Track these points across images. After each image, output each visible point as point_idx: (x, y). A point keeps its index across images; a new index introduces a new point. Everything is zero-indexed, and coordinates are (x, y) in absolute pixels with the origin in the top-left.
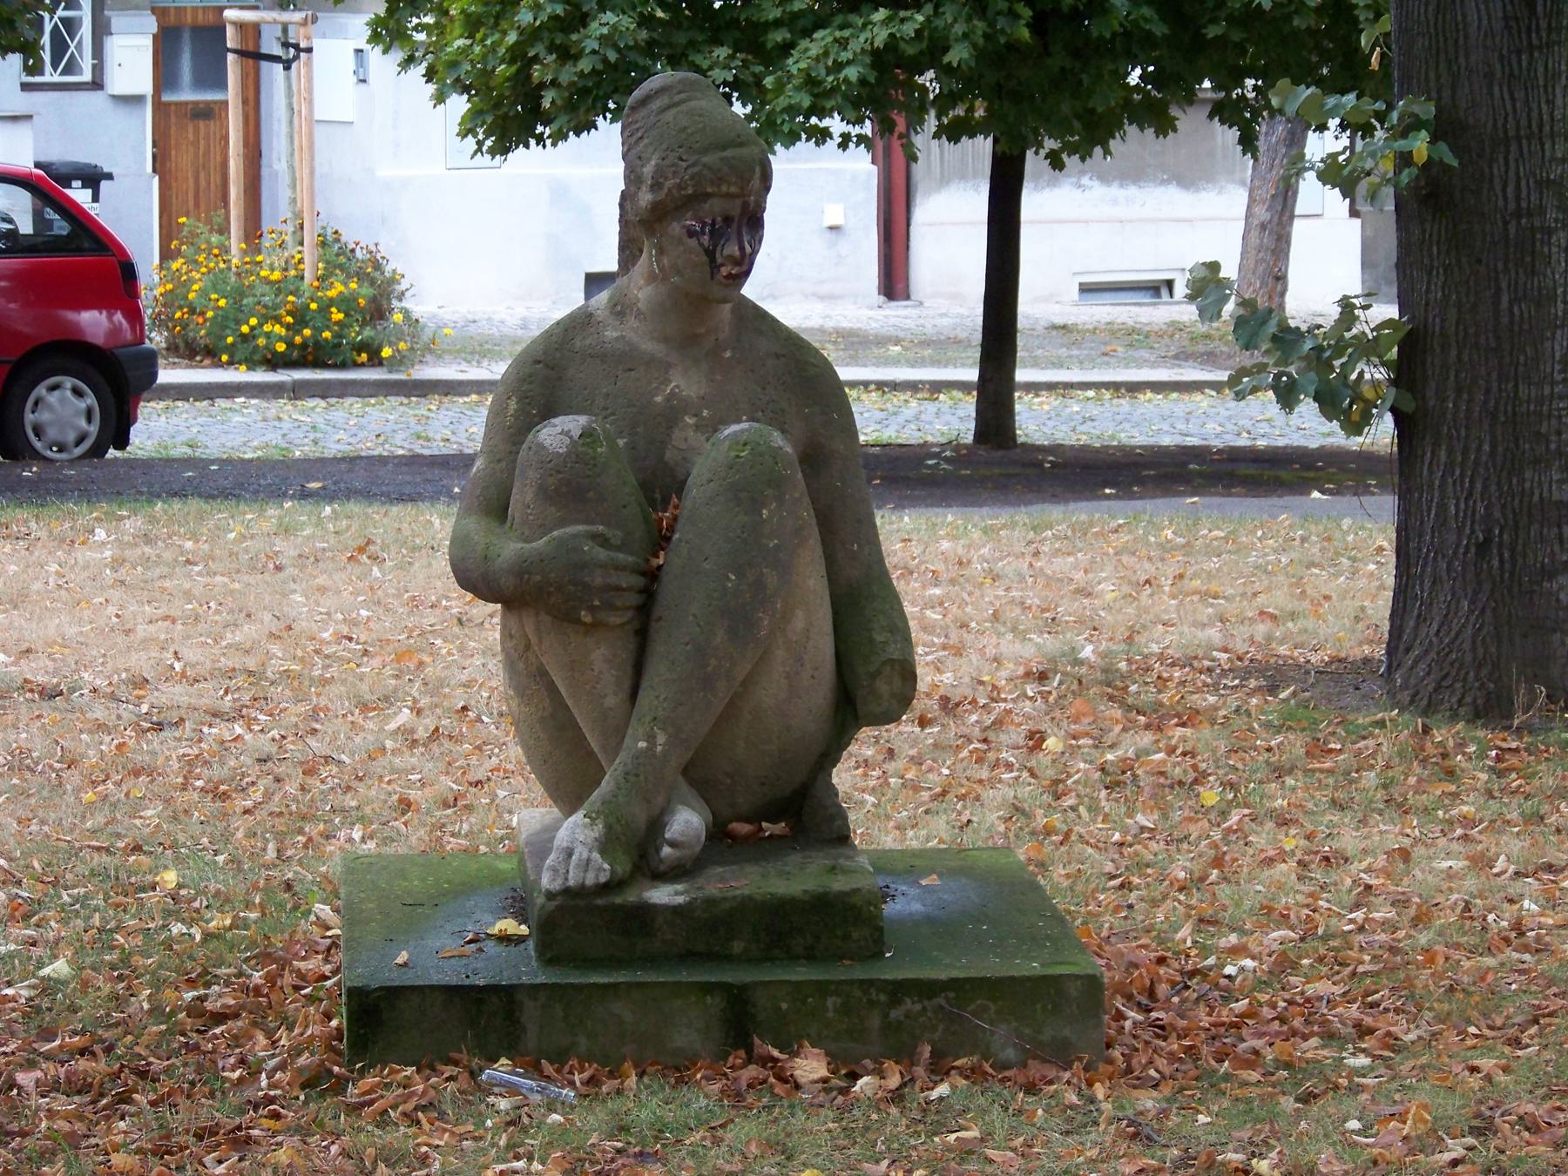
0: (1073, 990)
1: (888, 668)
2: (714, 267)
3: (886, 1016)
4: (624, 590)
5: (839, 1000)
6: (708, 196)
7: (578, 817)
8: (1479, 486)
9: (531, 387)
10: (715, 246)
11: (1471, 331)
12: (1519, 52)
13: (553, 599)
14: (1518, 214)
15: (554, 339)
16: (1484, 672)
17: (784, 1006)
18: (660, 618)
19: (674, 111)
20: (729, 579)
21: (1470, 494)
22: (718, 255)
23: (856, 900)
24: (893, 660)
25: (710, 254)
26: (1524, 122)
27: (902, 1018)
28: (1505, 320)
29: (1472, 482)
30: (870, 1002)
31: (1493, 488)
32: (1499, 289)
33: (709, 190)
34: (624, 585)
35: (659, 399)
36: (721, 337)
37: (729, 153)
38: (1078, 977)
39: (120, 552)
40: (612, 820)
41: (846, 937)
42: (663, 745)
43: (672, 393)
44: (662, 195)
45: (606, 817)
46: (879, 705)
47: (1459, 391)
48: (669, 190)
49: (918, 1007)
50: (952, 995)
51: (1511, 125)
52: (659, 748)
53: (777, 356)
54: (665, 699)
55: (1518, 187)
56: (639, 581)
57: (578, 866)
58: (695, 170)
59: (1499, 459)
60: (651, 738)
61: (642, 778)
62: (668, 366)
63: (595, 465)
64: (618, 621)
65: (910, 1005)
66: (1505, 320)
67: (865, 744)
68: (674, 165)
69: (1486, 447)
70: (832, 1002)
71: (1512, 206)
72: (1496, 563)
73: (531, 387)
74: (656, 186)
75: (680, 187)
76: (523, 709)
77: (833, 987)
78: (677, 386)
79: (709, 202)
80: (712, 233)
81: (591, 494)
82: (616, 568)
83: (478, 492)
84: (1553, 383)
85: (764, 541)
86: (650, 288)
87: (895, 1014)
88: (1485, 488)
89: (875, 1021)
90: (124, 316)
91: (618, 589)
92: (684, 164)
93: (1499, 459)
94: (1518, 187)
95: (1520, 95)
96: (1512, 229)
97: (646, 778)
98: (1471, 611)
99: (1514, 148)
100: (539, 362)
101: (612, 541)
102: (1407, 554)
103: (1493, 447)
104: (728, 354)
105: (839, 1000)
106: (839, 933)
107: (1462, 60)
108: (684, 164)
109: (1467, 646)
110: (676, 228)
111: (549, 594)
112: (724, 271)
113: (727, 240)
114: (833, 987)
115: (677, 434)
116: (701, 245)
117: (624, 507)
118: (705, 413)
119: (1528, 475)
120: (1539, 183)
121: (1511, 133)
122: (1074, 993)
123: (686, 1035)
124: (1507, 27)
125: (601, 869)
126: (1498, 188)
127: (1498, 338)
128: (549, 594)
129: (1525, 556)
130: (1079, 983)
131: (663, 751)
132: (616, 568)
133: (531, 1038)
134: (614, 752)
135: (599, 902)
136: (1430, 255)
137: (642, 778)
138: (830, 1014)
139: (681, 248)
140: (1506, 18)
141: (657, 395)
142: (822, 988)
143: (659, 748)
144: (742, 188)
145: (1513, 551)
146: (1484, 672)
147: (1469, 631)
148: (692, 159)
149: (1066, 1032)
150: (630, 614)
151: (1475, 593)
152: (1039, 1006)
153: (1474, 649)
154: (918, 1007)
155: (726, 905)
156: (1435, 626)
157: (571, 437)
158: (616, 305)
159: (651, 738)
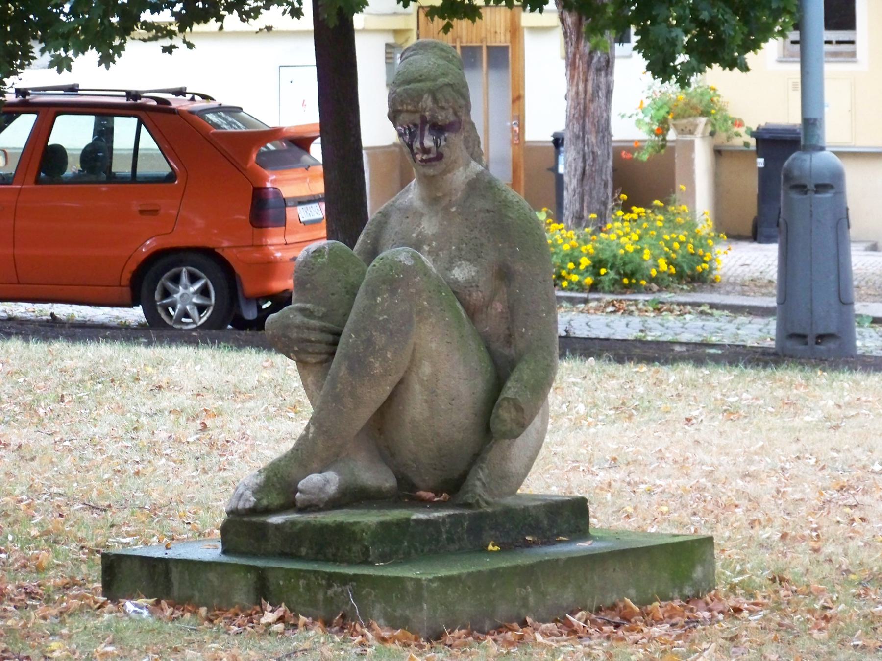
0: (410, 586)
1: (506, 403)
3: (326, 593)
4: (312, 342)
5: (305, 582)
10: (412, 142)
17: (281, 583)
20: (351, 337)
23: (357, 529)
24: (508, 398)
27: (333, 595)
30: (319, 584)
34: (313, 339)
35: (414, 235)
36: (454, 199)
37: (412, 86)
38: (411, 579)
40: (272, 474)
41: (350, 551)
42: (313, 433)
43: (421, 232)
45: (268, 472)
46: (504, 425)
49: (340, 590)
50: (355, 584)
52: (310, 435)
53: (488, 211)
56: (330, 338)
61: (300, 452)
62: (422, 215)
63: (313, 269)
64: (314, 361)
65: (336, 588)
70: (302, 582)
77: (302, 574)
78: (424, 228)
79: (402, 115)
80: (410, 133)
81: (308, 286)
82: (308, 329)
85: (377, 316)
87: (330, 593)
89: (321, 597)
90: (638, 206)
91: (310, 341)
97: (302, 452)
101: (316, 314)
104: (454, 209)
105: (305, 582)
106: (347, 547)
114: (302, 574)
117: (333, 294)
118: (434, 244)
122: (410, 589)
123: (241, 596)
125: (248, 500)
130: (412, 583)
131: (313, 436)
132: (308, 329)
133: (176, 591)
135: (245, 519)
137: (300, 452)
138: (301, 590)
141: (413, 233)
142: (298, 574)
143: (310, 435)
149: (407, 612)
152: (394, 595)
154: (340, 590)
155: (299, 526)
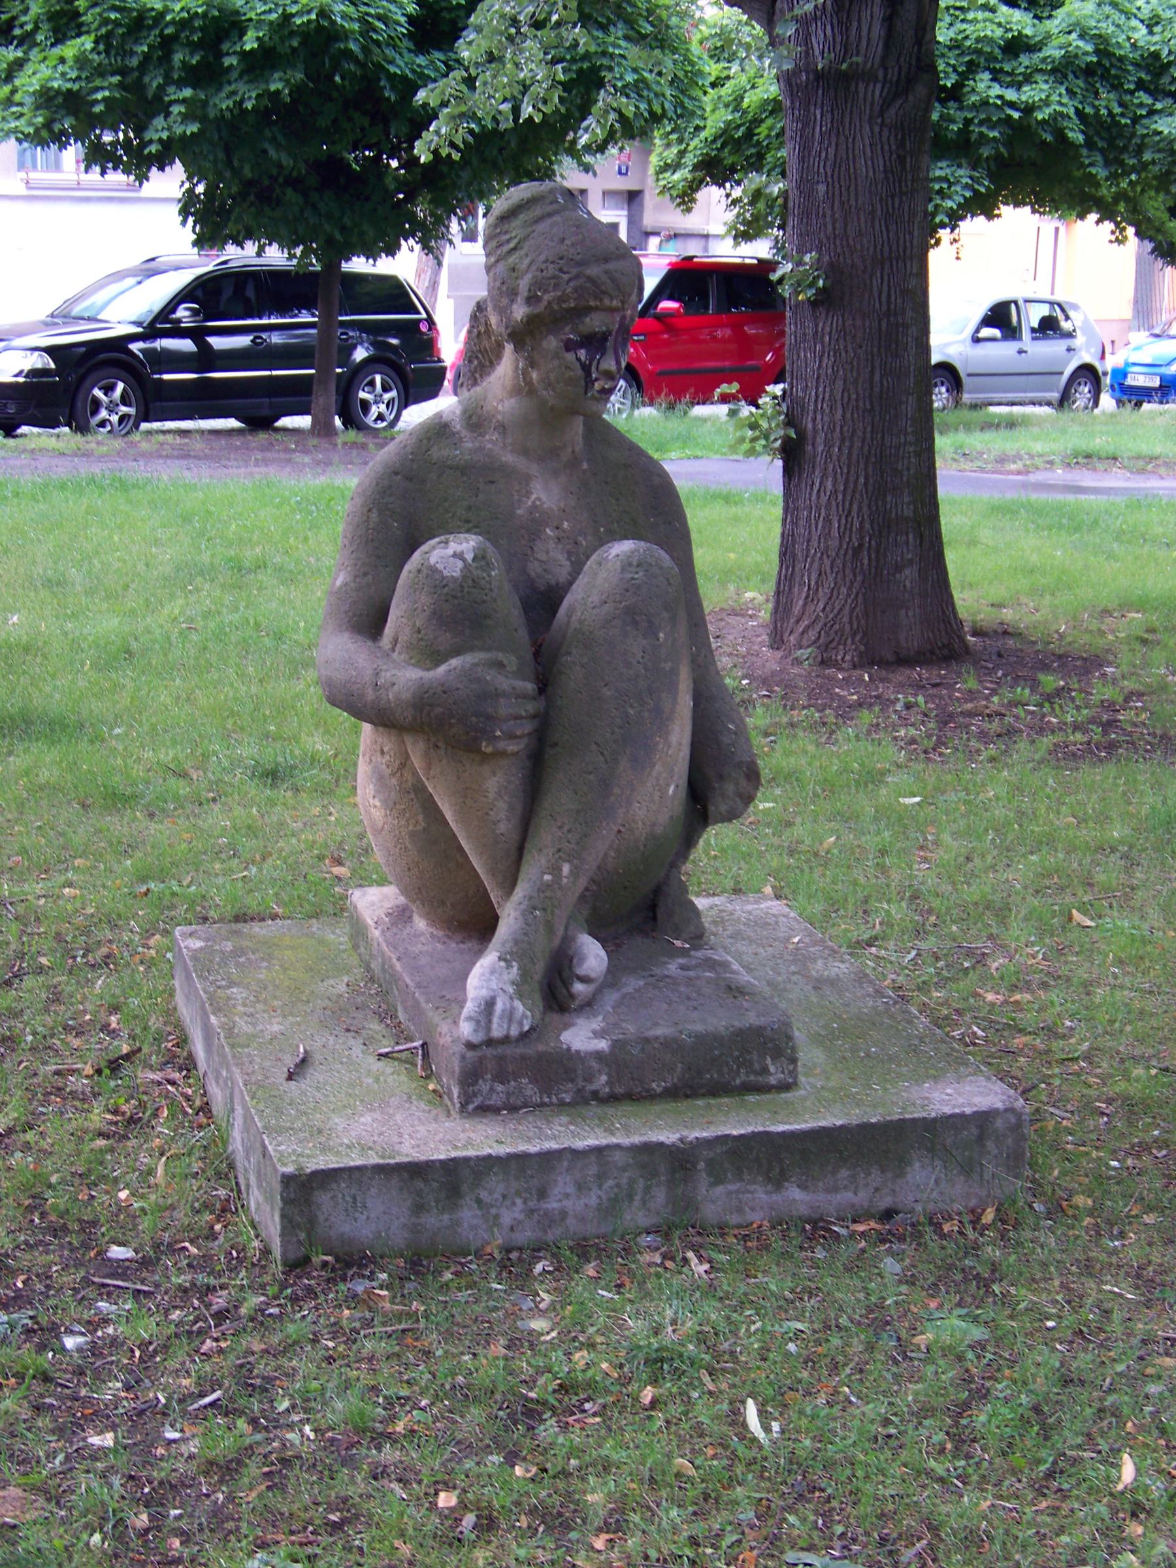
2: (589, 382)
6: (589, 310)
7: (489, 959)
8: (855, 507)
9: (391, 499)
11: (854, 396)
12: (893, 196)
13: (454, 730)
14: (888, 314)
15: (409, 449)
16: (858, 638)
18: (556, 744)
19: (549, 221)
21: (849, 512)
22: (593, 369)
25: (586, 369)
26: (894, 248)
28: (877, 390)
29: (851, 504)
31: (865, 509)
32: (873, 368)
33: (592, 303)
39: (540, 1234)
43: (534, 506)
44: (540, 308)
47: (843, 440)
48: (549, 303)
51: (886, 249)
54: (569, 831)
55: (889, 296)
57: (501, 1018)
58: (580, 282)
59: (870, 488)
60: (555, 870)
66: (877, 390)
67: (715, 837)
68: (554, 277)
69: (862, 480)
71: (884, 308)
72: (866, 561)
73: (391, 499)
74: (531, 300)
75: (561, 300)
76: (390, 819)
78: (538, 499)
83: (346, 608)
84: (906, 434)
86: (513, 401)
88: (860, 509)
92: (566, 277)
93: (870, 488)
94: (889, 296)
95: (893, 227)
96: (884, 325)
98: (849, 595)
99: (887, 266)
100: (396, 473)
102: (794, 556)
103: (866, 478)
107: (853, 202)
108: (566, 277)
109: (846, 620)
110: (552, 343)
111: (451, 725)
112: (597, 386)
113: (603, 355)
115: (538, 546)
116: (578, 359)
118: (566, 525)
119: (889, 499)
120: (902, 292)
121: (886, 254)
124: (887, 178)
126: (876, 295)
127: (872, 403)
128: (451, 725)
129: (885, 556)
134: (510, 883)
136: (822, 344)
139: (556, 363)
140: (885, 171)
144: (623, 302)
145: (877, 552)
146: (858, 638)
147: (847, 607)
148: (574, 271)
150: (525, 741)
151: (852, 583)
153: (851, 623)
156: (821, 605)
157: (464, 560)
158: (470, 417)
159: (555, 870)
